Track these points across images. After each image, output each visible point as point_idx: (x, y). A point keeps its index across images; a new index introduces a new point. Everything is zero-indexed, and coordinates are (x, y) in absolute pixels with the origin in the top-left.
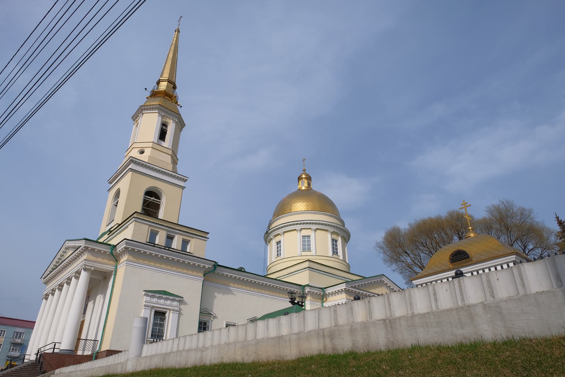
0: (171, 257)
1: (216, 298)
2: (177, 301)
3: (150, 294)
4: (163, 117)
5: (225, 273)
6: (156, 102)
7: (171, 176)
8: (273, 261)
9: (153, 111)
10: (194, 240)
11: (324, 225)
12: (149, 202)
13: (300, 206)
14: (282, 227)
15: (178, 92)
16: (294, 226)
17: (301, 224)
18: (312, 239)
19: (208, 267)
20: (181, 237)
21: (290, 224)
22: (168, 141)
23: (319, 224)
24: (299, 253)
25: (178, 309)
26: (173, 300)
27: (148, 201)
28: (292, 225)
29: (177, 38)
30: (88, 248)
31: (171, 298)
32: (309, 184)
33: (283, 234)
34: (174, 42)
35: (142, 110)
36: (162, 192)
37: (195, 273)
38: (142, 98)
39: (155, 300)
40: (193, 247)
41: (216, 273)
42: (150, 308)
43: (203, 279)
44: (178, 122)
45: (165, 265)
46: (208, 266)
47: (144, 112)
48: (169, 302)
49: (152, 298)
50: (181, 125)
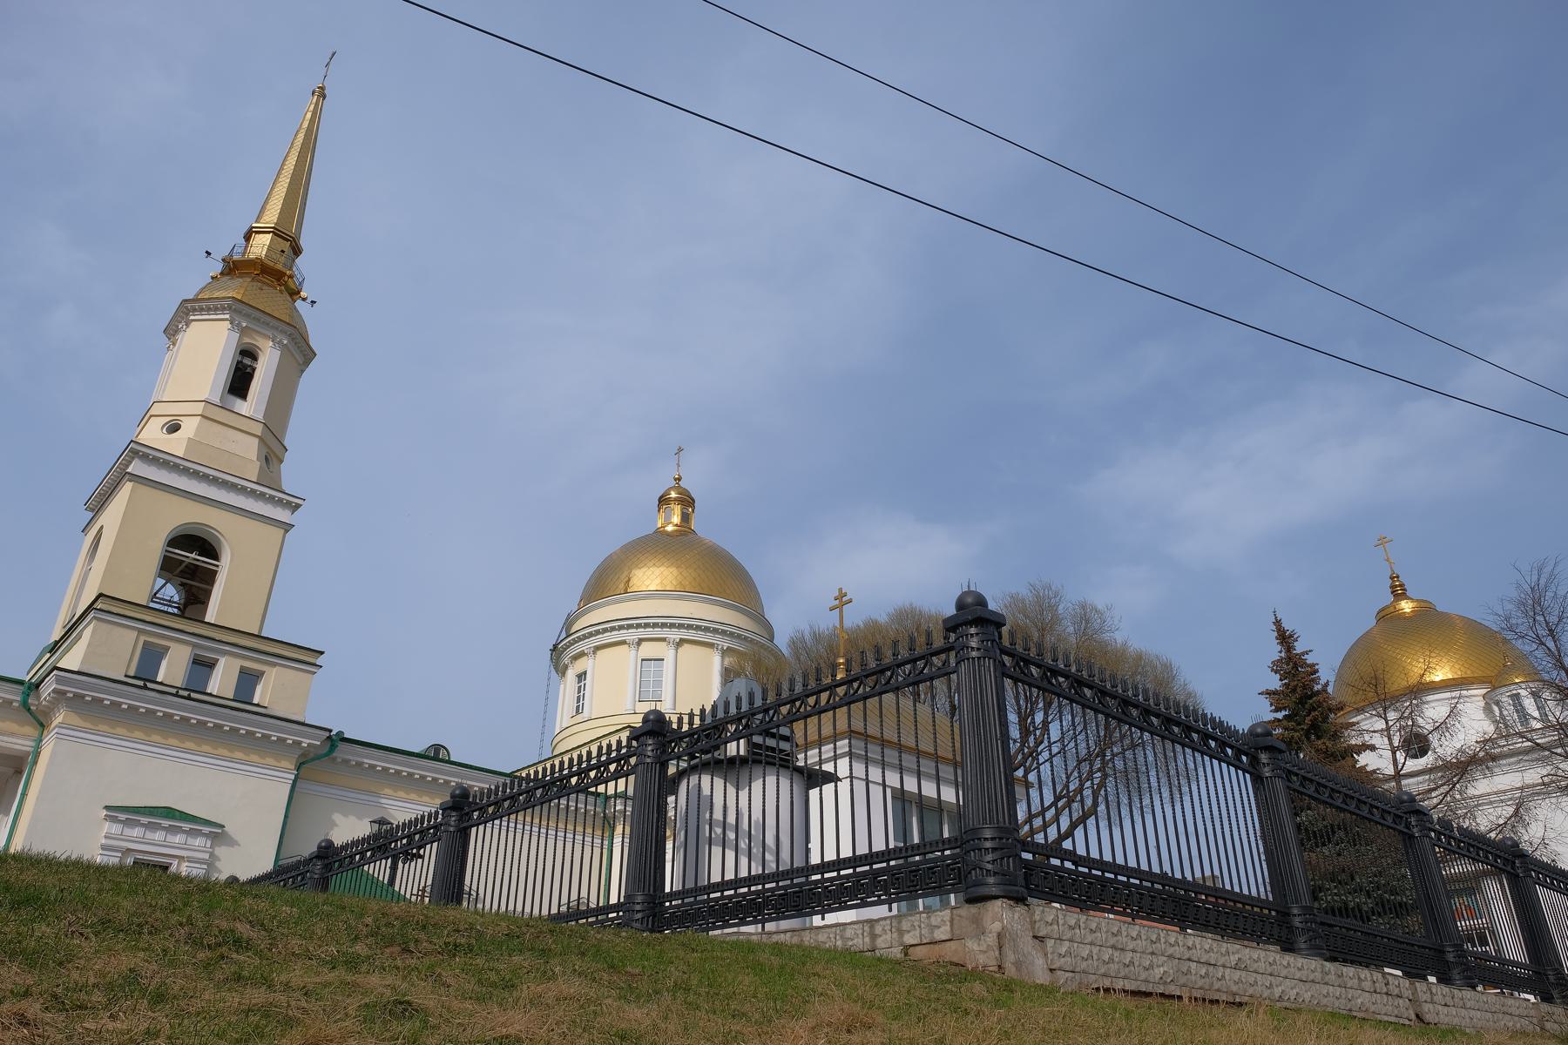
0: (194, 718)
1: (336, 829)
2: (205, 835)
3: (123, 817)
4: (243, 332)
5: (366, 761)
6: (234, 289)
7: (261, 496)
8: (565, 726)
9: (217, 314)
10: (275, 670)
11: (702, 630)
12: (184, 565)
13: (651, 577)
14: (591, 635)
15: (303, 265)
16: (622, 632)
17: (639, 626)
18: (668, 665)
19: (309, 745)
20: (237, 664)
21: (637, 624)
22: (254, 398)
23: (690, 627)
24: (629, 707)
25: (207, 856)
26: (192, 833)
27: (184, 561)
28: (617, 630)
29: (314, 113)
30: (65, 693)
31: (186, 826)
32: (685, 518)
33: (594, 653)
34: (306, 125)
35: (188, 310)
36: (222, 539)
37: (270, 761)
38: (198, 275)
39: (137, 832)
40: (274, 689)
41: (339, 760)
42: (120, 855)
43: (293, 777)
44: (290, 347)
45: (194, 743)
46: (308, 741)
47: (192, 318)
48: (178, 839)
49: (128, 827)
50: (300, 352)
